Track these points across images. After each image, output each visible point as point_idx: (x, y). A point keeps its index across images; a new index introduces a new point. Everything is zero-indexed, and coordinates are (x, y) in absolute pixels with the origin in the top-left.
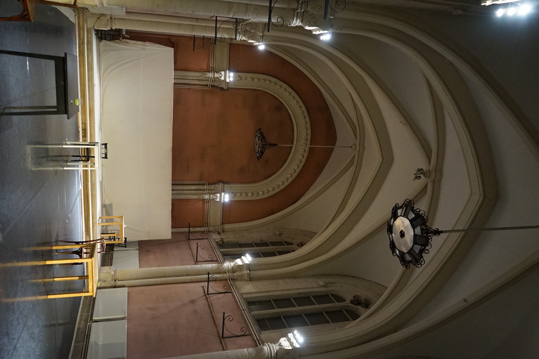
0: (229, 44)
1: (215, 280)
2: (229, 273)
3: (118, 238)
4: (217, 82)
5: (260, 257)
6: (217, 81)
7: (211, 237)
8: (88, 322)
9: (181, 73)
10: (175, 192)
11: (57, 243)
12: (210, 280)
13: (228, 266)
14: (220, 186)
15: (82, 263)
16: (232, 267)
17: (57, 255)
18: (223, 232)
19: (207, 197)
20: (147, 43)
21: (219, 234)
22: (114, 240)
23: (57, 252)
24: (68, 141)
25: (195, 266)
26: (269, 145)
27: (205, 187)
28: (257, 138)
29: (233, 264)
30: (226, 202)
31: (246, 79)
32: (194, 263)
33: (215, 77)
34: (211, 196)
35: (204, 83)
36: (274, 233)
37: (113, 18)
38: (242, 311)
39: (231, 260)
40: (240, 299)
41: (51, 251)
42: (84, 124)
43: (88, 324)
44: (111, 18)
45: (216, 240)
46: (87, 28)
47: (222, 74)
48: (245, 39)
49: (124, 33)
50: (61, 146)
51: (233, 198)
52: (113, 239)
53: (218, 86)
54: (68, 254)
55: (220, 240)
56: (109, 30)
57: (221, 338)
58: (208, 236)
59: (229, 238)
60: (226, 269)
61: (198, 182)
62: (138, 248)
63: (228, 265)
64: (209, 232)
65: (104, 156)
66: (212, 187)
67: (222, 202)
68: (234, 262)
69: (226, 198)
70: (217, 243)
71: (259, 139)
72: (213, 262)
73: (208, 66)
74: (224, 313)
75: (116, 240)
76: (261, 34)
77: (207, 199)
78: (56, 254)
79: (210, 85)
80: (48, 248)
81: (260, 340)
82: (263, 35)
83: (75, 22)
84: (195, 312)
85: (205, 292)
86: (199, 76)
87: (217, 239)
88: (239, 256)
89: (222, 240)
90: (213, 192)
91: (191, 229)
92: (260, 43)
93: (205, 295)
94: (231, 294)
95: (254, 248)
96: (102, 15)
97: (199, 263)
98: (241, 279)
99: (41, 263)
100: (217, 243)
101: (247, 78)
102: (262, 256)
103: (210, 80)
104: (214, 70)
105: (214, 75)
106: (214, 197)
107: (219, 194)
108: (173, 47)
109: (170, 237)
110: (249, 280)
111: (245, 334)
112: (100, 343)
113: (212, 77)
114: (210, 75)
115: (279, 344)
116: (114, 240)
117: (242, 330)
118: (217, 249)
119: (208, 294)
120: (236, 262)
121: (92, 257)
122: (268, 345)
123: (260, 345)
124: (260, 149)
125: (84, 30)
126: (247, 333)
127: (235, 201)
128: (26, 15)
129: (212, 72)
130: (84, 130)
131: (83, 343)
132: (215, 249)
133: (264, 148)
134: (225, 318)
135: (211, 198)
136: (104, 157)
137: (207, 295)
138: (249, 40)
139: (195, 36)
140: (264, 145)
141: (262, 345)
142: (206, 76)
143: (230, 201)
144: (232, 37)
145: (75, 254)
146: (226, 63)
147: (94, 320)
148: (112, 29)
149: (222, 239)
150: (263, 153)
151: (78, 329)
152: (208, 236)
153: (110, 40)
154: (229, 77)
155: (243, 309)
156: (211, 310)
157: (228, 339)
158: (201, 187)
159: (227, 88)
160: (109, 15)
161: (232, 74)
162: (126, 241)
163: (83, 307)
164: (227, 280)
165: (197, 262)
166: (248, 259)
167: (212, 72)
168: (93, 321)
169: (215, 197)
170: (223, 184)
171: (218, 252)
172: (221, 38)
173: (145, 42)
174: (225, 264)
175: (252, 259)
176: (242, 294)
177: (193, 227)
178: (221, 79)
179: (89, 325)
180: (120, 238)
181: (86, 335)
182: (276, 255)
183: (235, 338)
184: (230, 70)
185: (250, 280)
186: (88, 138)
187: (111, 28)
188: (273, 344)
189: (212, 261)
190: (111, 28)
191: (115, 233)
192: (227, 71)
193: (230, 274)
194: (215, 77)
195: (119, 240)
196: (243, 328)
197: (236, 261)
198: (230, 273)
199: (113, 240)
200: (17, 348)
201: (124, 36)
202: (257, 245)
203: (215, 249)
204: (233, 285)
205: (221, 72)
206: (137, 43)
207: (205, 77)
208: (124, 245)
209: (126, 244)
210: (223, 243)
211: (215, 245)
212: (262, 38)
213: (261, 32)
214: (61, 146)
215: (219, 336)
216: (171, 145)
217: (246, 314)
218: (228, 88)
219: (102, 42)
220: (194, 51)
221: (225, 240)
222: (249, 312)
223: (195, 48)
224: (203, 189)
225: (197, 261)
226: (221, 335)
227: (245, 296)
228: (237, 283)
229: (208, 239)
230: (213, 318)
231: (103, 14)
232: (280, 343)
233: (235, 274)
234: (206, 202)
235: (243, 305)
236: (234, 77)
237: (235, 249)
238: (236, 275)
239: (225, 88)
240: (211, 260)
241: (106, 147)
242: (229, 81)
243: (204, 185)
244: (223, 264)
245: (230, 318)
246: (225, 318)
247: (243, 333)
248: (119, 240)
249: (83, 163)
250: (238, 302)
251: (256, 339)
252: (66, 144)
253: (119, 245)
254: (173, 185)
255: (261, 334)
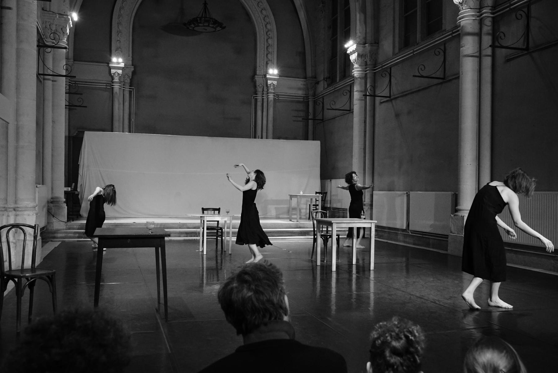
0: (75, 62)
1: (374, 87)
2: (367, 71)
3: (316, 202)
4: (126, 79)
5: (349, 30)
6: (124, 80)
7: (321, 93)
8: (408, 234)
9: (116, 124)
10: (264, 134)
11: (314, 262)
12: (373, 94)
13: (358, 71)
14: (259, 80)
15: (338, 235)
16: (359, 65)
17: (326, 261)
18: (315, 78)
19: (271, 97)
20: (81, 163)
21: (318, 83)
22: (318, 205)
23: (324, 261)
24: (199, 249)
25: (354, 113)
26: (205, 12)
27: (259, 98)
28: (196, 29)
29: (356, 65)
30: (278, 71)
31: (120, 42)
32: (351, 114)
33: (118, 81)
34: (270, 91)
35: (127, 95)
36: (321, 11)
37: (52, 200)
38: (414, 53)
39: (351, 67)
40: (400, 57)
41: (322, 266)
42: (180, 234)
43: (410, 234)
44: (52, 202)
45: (326, 86)
46: (66, 230)
47: (114, 72)
48: (66, 39)
49: (69, 189)
50: (205, 256)
51: (273, 64)
52: (316, 207)
53: (131, 78)
54: (326, 252)
55: (325, 82)
56: (67, 206)
57: (445, 80)
58: (319, 96)
59: (323, 71)
60: (362, 73)
61: (253, 107)
62: (329, 180)
63: (356, 72)
64: (314, 95)
65: (217, 212)
66: (260, 90)
67: (278, 78)
68: (354, 63)
69: (273, 72)
70: (329, 85)
71: (198, 26)
72: (352, 91)
73: (105, 90)
74: (414, 76)
75: (317, 203)
76: (58, 17)
77: (274, 96)
78: (325, 262)
79: (130, 89)
80: (319, 268)
81: (453, 30)
82: (59, 14)
83: (59, 241)
84: (409, 113)
85: (387, 101)
86: (119, 102)
87: (324, 85)
88: (347, 56)
89: (325, 79)
90: (265, 89)
91: (310, 117)
92: (69, 19)
93: (391, 100)
94: (392, 69)
95: (339, 37)
96: (49, 212)
97: (351, 109)
98: (375, 54)
99: (334, 275)
100: (329, 85)
101: (119, 39)
102: (349, 27)
103: (124, 87)
104: (110, 82)
105: (116, 82)
106: (272, 88)
107: (268, 81)
108: (83, 133)
109: (318, 143)
110: (377, 45)
111: (443, 50)
112: (432, 222)
113: (120, 86)
114: (116, 87)
115: (460, 5)
116: (318, 205)
117: (437, 53)
118: (336, 86)
119: (390, 97)
120: (354, 61)
121: (331, 223)
122: (460, 19)
123: (458, 31)
124: (210, 25)
125: (69, 232)
126: (442, 47)
127: (277, 63)
128: (48, 277)
129: (113, 85)
130: (187, 234)
131: (431, 240)
132: (337, 87)
133: (209, 19)
134: (420, 75)
135: (273, 91)
136: (218, 211)
137: (391, 98)
138: (67, 33)
139: (67, 104)
140: (206, 19)
141: (459, 28)
142: (118, 92)
143: (277, 69)
144: (65, 57)
145: (328, 243)
146: (102, 67)
147: (406, 227)
148: (66, 202)
149: (324, 79)
150: (216, 21)
151: (414, 244)
152: (319, 96)
153: (80, 206)
154: (118, 63)
155: (414, 52)
156: (409, 94)
157: (446, 72)
158: (259, 104)
159: (133, 67)
160: (49, 205)
161: (114, 60)
162: (319, 193)
163: (391, 240)
164: (375, 73)
165: (351, 111)
166: (351, 46)
167: (113, 85)
168: (407, 229)
169: (272, 86)
170: (256, 76)
171: (340, 84)
172: (67, 70)
173: (79, 165)
174: (355, 75)
175: (351, 39)
176: (394, 54)
177: (308, 115)
178: (121, 73)
179: (411, 233)
180: (316, 199)
181: (421, 237)
182: (349, 9)
183: (447, 63)
184: (109, 61)
185: (378, 43)
186: (197, 231)
187: (64, 202)
188: (460, 13)
189: (351, 92)
190: (64, 202)
191: (310, 205)
192: (110, 65)
193: (368, 69)
194: (118, 81)
195: (318, 201)
196: (436, 52)
197: (352, 61)
198: (367, 68)
199: (317, 207)
200: (421, 296)
201: (74, 189)
202: (334, 33)
203: (337, 87)
204: (382, 65)
205: (112, 73)
206: (81, 175)
207: (120, 94)
208: (325, 195)
209: (323, 193)
210: (329, 78)
211: (331, 88)
212: (64, 16)
213: (54, 16)
214: (205, 256)
215: (441, 83)
216: (206, 138)
217: (417, 49)
218: (132, 65)
219: (83, 215)
220: (86, 107)
221: (327, 75)
222: (417, 44)
223: (83, 105)
224: (261, 101)
225: (350, 110)
226: (441, 81)
227: (397, 50)
228: (381, 59)
229: (323, 96)
230: (419, 91)
231: (48, 211)
232: (460, 3)
233: (369, 63)
234: (278, 97)
235: (408, 53)
236: (118, 56)
237: (338, 63)
238: (370, 61)
239: (133, 69)
240: (349, 94)
241: (207, 209)
242: (124, 64)
243: (256, 100)
244: (356, 77)
245: (421, 69)
246: (421, 75)
247: (442, 53)
248: (318, 201)
249: (224, 237)
250: (404, 58)
251: (450, 36)
252: (203, 251)
253: (324, 200)
254: (255, 137)
255: (446, 30)
